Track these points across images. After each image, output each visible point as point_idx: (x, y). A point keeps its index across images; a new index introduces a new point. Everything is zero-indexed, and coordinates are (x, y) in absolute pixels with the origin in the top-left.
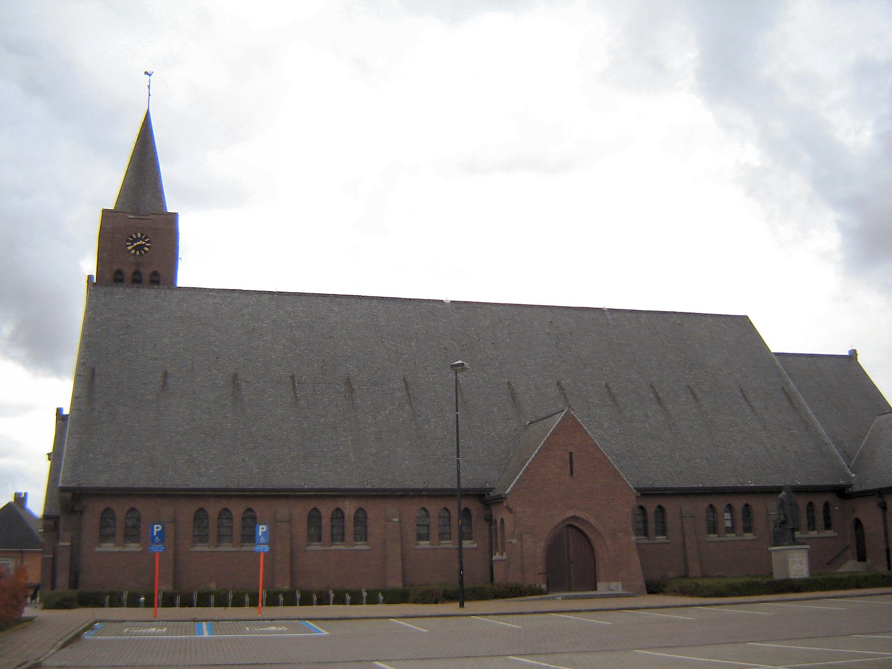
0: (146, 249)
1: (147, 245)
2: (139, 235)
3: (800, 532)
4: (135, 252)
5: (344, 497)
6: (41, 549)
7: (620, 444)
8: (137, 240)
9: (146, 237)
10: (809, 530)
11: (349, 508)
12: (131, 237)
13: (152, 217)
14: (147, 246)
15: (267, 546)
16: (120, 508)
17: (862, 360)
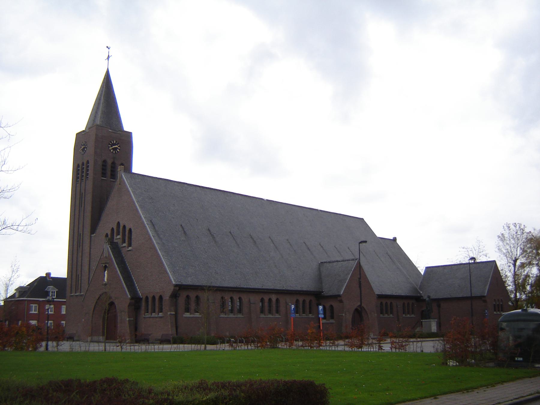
0: (118, 150)
1: (119, 148)
2: (115, 142)
3: (312, 315)
4: (113, 151)
5: (272, 293)
7: (526, 291)
8: (114, 145)
9: (118, 144)
10: (185, 312)
11: (274, 298)
12: (111, 143)
14: (119, 149)
15: (322, 315)
16: (193, 295)
17: (398, 241)
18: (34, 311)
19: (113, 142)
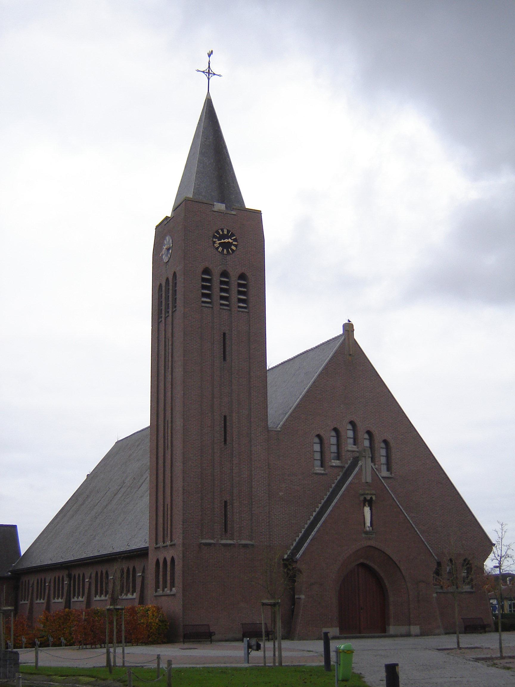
0: (233, 248)
1: (234, 243)
4: (223, 250)
6: (229, 235)
9: (233, 235)
12: (218, 233)
13: (101, 654)
14: (234, 245)
18: (513, 610)
19: (221, 233)
